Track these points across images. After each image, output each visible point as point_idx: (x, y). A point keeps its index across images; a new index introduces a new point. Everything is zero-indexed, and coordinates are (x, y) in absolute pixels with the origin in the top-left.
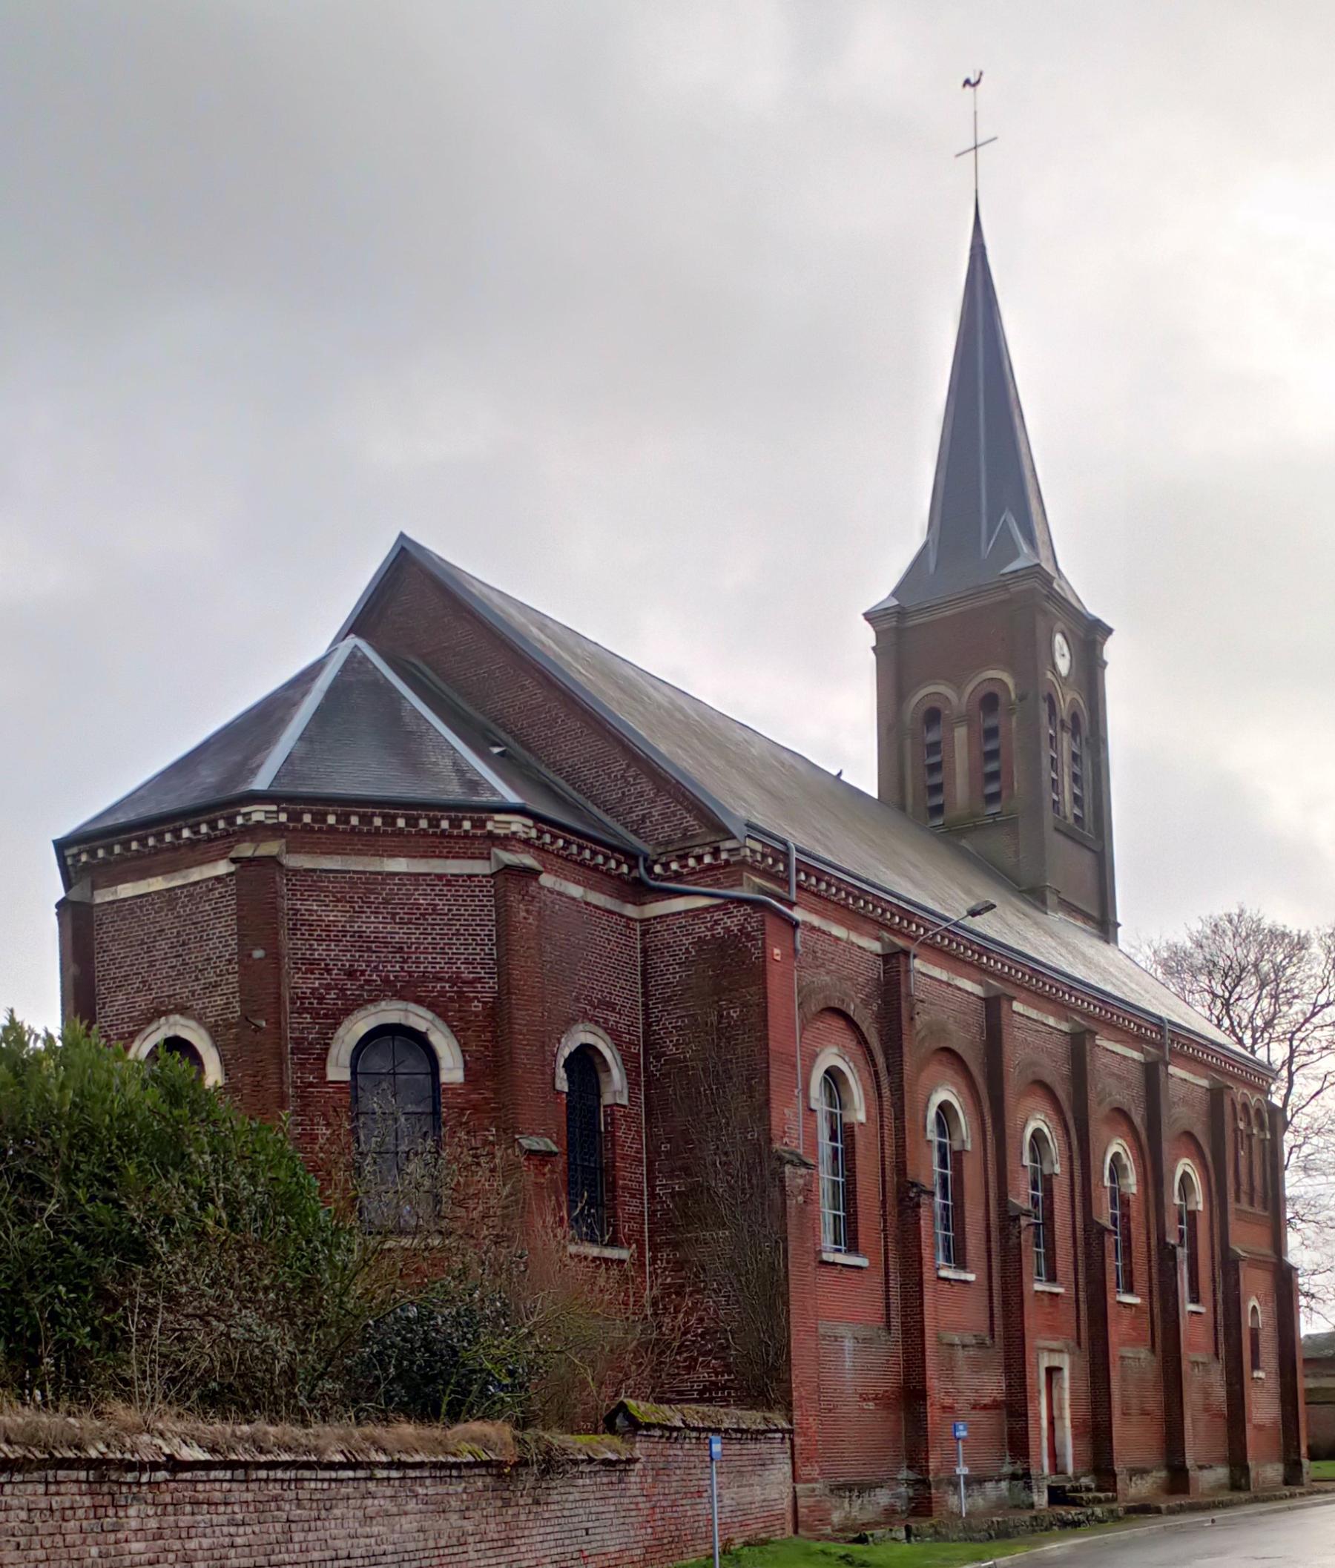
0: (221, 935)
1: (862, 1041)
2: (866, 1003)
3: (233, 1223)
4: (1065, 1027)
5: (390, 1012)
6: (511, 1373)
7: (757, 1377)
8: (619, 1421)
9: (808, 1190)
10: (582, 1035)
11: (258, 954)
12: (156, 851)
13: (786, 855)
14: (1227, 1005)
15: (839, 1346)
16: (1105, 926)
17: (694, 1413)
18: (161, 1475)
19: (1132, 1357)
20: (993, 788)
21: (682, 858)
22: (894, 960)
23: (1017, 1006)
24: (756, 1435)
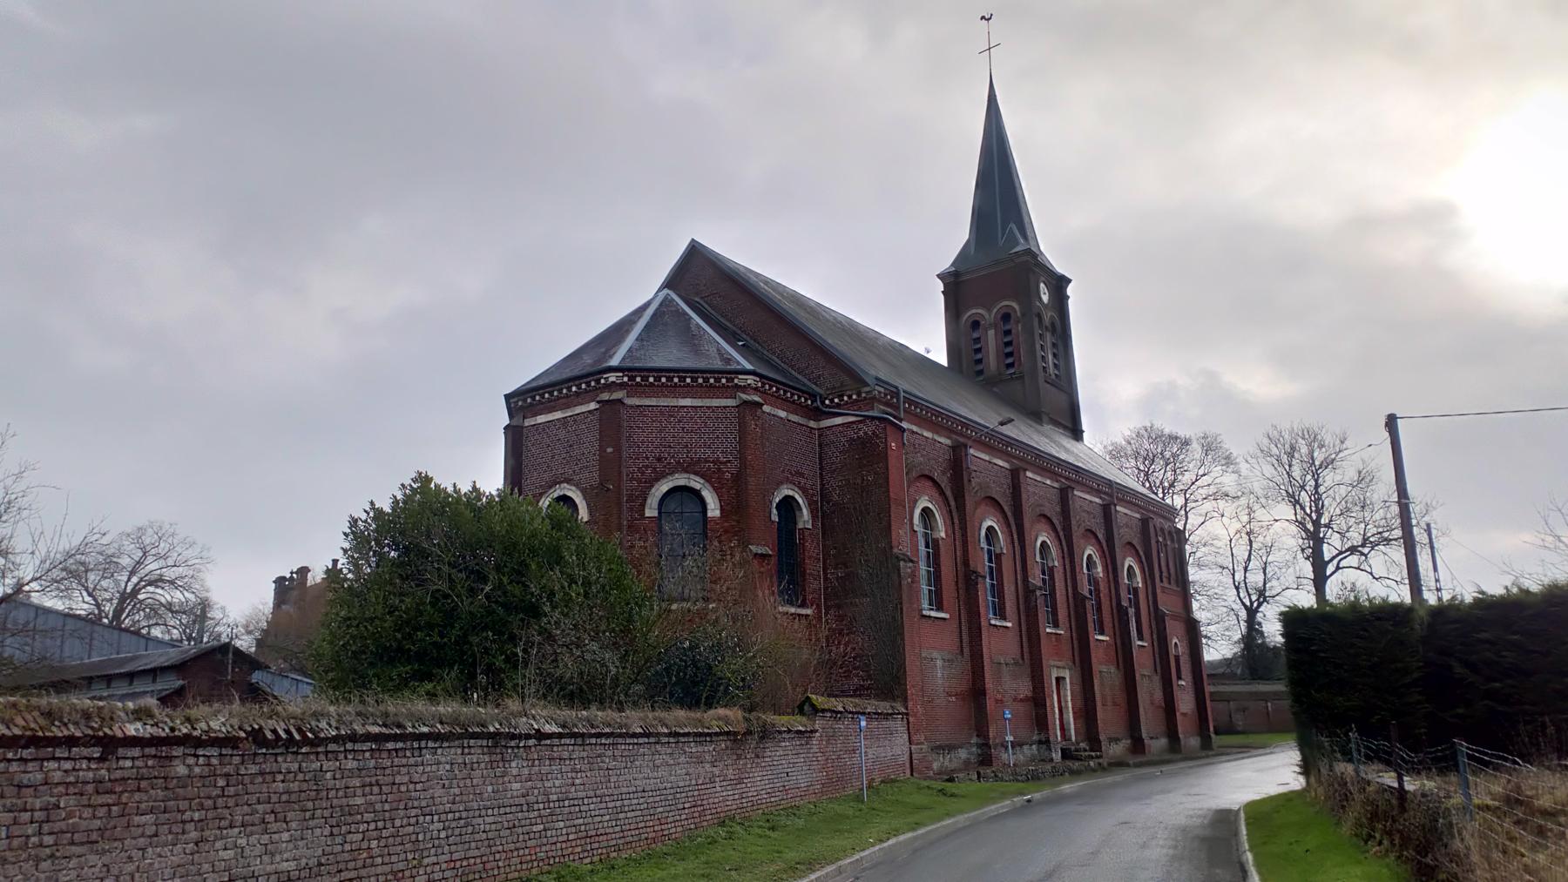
0: (590, 443)
1: (942, 493)
2: (944, 473)
3: (586, 595)
4: (1056, 485)
5: (680, 480)
6: (743, 680)
7: (884, 681)
8: (806, 707)
9: (914, 575)
10: (786, 491)
11: (610, 450)
12: (558, 398)
13: (897, 394)
14: (1147, 474)
15: (934, 664)
16: (1077, 433)
17: (851, 703)
18: (532, 742)
19: (1106, 673)
20: (1010, 360)
21: (841, 397)
22: (958, 451)
23: (1029, 474)
24: (887, 716)
